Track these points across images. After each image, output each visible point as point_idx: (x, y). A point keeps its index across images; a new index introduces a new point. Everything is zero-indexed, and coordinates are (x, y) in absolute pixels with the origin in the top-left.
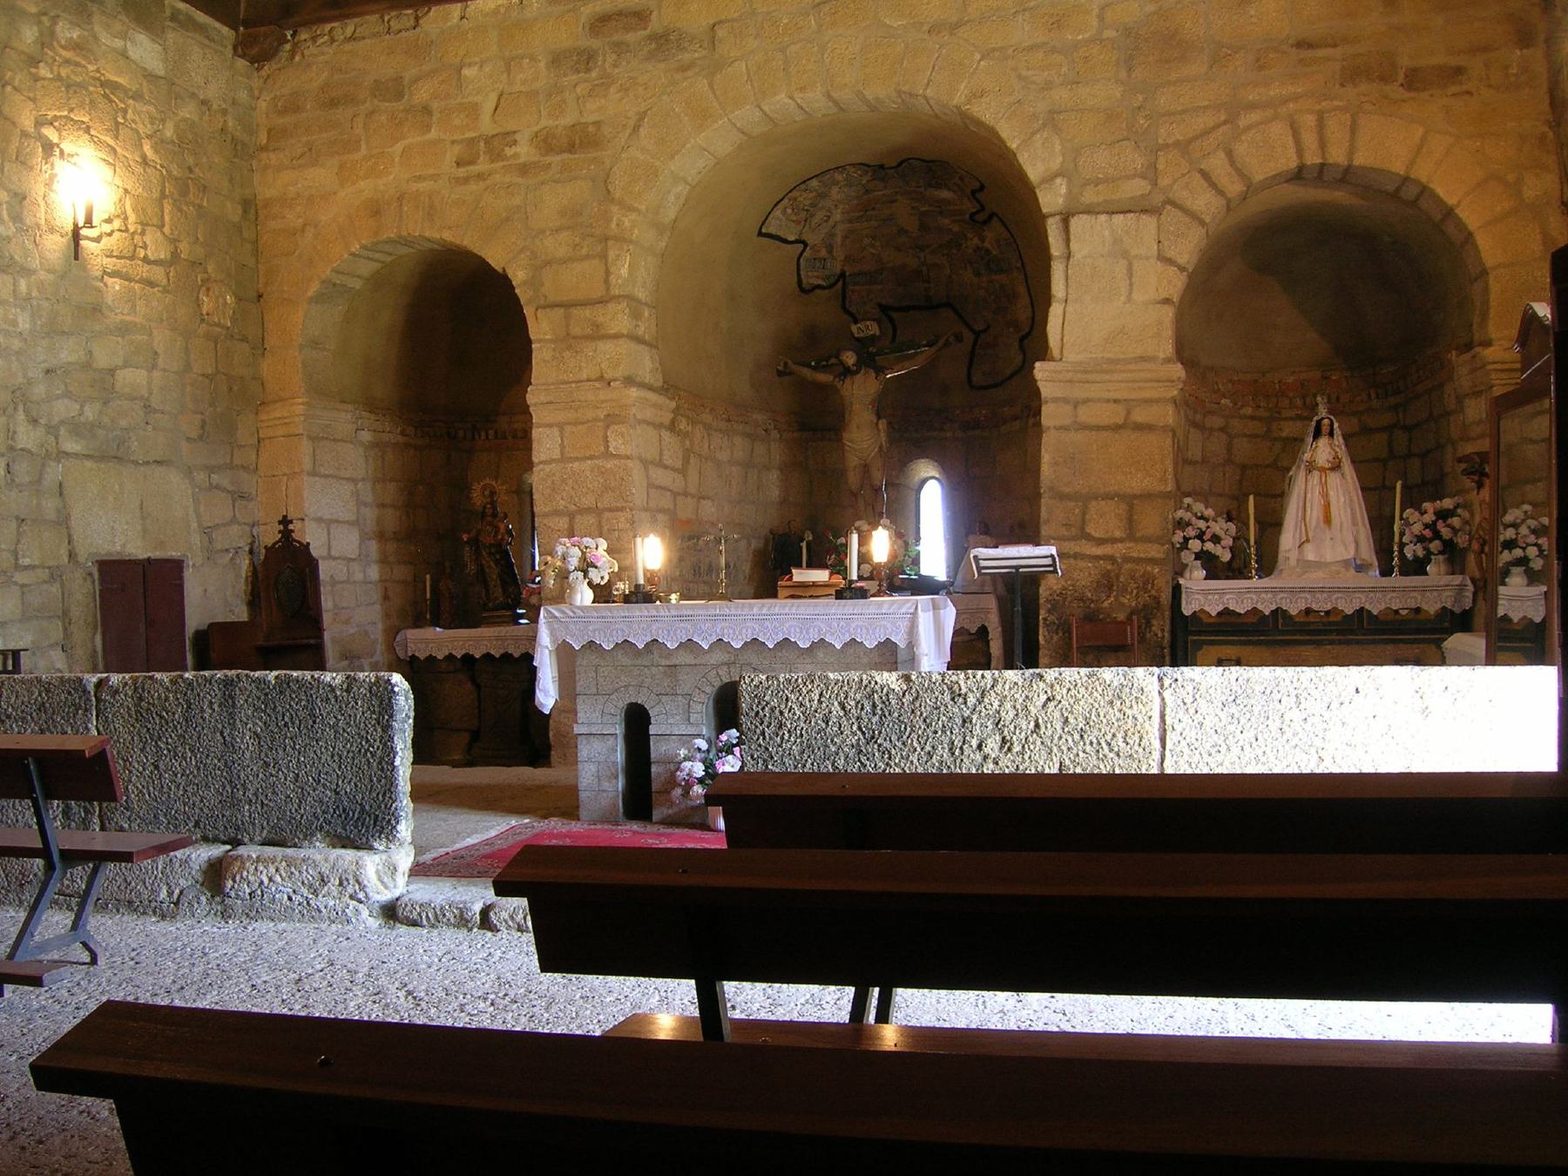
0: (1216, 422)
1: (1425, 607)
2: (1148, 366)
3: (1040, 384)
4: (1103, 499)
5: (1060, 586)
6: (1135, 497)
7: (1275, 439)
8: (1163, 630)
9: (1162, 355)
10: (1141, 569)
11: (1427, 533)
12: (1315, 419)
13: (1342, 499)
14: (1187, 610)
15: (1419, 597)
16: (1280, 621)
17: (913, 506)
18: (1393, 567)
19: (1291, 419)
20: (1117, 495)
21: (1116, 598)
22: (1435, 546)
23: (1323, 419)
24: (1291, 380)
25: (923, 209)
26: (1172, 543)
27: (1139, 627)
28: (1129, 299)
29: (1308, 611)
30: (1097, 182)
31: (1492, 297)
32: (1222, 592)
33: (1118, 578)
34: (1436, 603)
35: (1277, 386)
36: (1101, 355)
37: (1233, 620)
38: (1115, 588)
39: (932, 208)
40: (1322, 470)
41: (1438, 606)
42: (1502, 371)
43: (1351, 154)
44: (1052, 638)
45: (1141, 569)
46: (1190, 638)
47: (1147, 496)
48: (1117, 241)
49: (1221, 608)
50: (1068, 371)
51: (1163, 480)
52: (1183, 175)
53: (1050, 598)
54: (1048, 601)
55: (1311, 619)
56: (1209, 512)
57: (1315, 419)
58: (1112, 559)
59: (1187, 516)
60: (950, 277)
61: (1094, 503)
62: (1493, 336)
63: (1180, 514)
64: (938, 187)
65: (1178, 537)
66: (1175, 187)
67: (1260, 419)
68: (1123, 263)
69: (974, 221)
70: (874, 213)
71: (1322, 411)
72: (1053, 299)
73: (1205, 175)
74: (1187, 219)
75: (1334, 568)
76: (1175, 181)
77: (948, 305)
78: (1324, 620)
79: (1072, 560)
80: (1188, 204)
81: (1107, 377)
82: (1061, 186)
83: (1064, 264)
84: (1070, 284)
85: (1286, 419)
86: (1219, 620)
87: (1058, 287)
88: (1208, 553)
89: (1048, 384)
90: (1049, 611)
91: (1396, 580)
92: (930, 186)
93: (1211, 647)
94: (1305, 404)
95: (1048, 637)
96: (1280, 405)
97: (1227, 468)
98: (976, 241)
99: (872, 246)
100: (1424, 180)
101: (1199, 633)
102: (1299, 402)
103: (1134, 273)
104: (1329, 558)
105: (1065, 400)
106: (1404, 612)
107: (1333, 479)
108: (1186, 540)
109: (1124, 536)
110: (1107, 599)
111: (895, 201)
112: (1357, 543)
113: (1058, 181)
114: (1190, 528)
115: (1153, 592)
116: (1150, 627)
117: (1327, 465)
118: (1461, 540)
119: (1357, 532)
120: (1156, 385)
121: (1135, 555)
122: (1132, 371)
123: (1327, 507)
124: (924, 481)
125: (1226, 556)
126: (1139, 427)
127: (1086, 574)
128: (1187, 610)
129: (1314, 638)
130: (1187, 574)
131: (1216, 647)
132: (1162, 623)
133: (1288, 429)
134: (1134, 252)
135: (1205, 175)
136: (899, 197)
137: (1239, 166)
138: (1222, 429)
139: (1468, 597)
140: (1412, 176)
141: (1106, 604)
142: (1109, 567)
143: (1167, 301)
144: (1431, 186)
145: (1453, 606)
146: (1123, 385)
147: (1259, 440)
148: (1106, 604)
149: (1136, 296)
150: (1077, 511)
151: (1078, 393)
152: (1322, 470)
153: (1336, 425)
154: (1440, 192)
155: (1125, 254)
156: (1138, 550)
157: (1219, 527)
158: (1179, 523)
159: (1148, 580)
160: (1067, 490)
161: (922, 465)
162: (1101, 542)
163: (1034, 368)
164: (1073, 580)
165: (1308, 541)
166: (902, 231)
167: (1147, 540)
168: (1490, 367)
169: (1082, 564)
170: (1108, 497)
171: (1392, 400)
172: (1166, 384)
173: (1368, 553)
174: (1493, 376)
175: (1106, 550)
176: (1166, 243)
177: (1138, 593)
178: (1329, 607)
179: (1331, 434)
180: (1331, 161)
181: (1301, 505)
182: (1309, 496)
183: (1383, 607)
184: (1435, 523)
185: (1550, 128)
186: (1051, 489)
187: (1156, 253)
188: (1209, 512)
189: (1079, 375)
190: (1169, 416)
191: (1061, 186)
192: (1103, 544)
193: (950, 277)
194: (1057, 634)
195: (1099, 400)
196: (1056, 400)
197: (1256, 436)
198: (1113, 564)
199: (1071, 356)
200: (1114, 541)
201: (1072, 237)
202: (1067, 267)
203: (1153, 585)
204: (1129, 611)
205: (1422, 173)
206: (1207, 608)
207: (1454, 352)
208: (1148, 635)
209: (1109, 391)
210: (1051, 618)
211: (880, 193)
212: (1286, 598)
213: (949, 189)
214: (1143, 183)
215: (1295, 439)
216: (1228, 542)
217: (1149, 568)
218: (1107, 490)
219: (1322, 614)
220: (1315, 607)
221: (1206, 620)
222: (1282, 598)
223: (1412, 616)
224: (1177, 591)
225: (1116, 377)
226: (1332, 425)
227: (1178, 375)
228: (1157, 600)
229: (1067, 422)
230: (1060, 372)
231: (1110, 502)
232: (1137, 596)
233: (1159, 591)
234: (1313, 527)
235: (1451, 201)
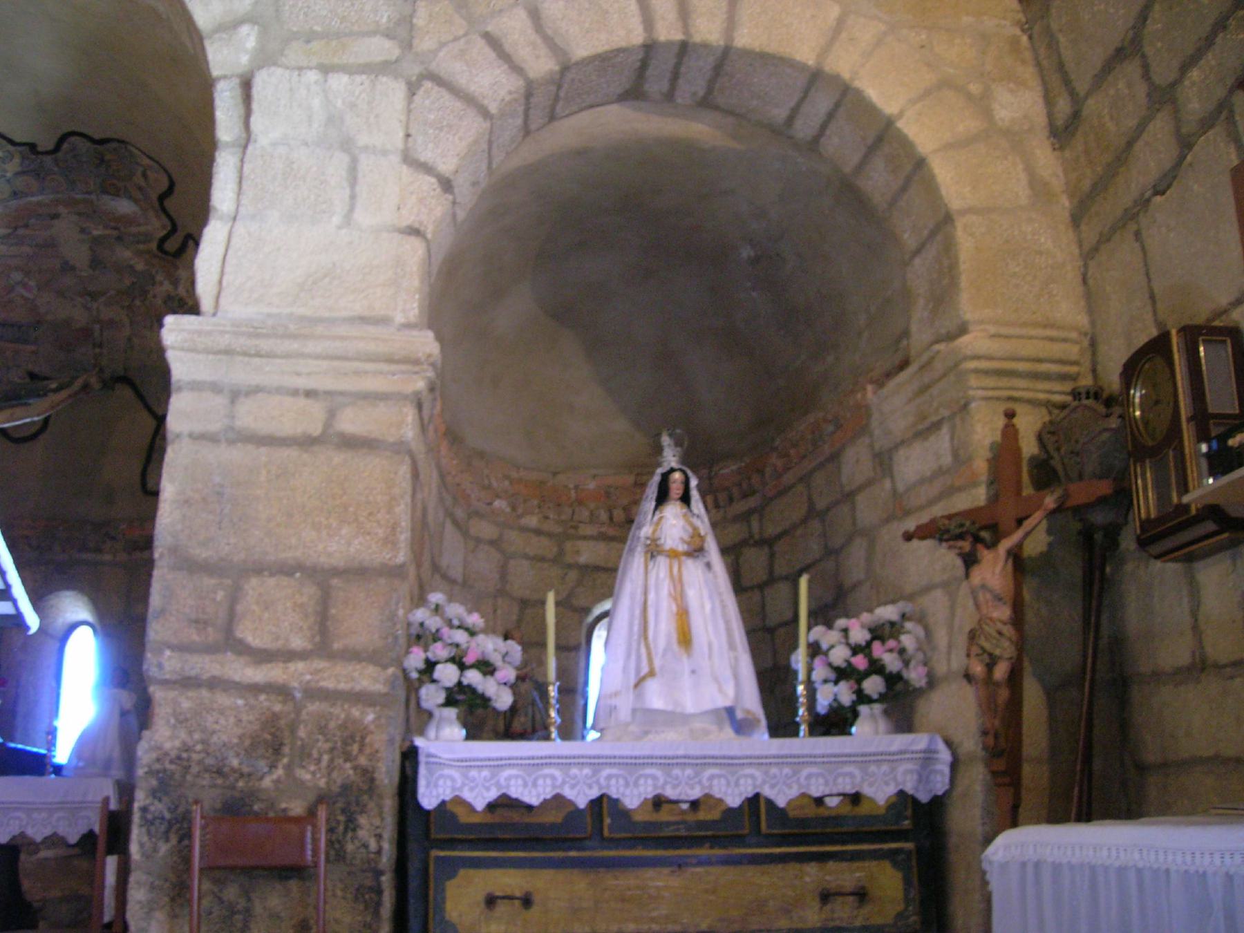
0: (486, 530)
1: (867, 791)
2: (372, 330)
3: (171, 356)
4: (272, 575)
5: (177, 743)
6: (336, 572)
7: (570, 566)
8: (379, 837)
9: (399, 318)
10: (339, 712)
11: (860, 662)
12: (659, 471)
13: (708, 607)
14: (428, 798)
15: (857, 772)
16: (607, 821)
17: (52, 660)
18: (798, 725)
19: (592, 538)
20: (300, 567)
21: (289, 768)
22: (873, 685)
23: (672, 470)
24: (592, 485)
25: (96, 233)
26: (404, 670)
27: (331, 830)
28: (348, 220)
29: (658, 802)
30: (310, 37)
31: (963, 256)
32: (497, 765)
33: (293, 729)
34: (887, 784)
35: (573, 492)
36: (288, 310)
37: (515, 817)
38: (286, 750)
39: (108, 232)
40: (673, 555)
41: (891, 790)
42: (986, 373)
43: (731, 24)
44: (155, 850)
45: (339, 712)
46: (435, 853)
47: (359, 573)
48: (333, 120)
49: (492, 795)
50: (223, 333)
51: (390, 541)
52: (456, 39)
53: (157, 766)
54: (151, 773)
55: (664, 816)
56: (475, 619)
57: (659, 471)
58: (282, 691)
59: (433, 623)
60: (129, 339)
61: (254, 581)
62: (968, 316)
63: (420, 614)
64: (117, 193)
65: (415, 660)
66: (441, 54)
67: (550, 535)
68: (341, 160)
69: (166, 253)
70: (27, 232)
71: (671, 458)
72: (212, 215)
73: (493, 42)
74: (459, 105)
75: (697, 725)
76: (442, 45)
77: (125, 380)
78: (691, 818)
79: (205, 693)
80: (462, 80)
81: (295, 346)
82: (249, 37)
83: (239, 155)
84: (245, 186)
85: (585, 538)
86: (489, 819)
87: (223, 194)
88: (470, 690)
89: (179, 353)
90: (154, 793)
91: (804, 744)
92: (105, 191)
93: (471, 872)
94: (611, 519)
95: (148, 845)
96: (576, 517)
97: (500, 601)
98: (167, 287)
99: (25, 286)
100: (846, 75)
101: (451, 843)
102: (604, 516)
103: (360, 175)
104: (690, 705)
105: (216, 388)
106: (832, 802)
107: (693, 571)
108: (430, 665)
109: (310, 647)
110: (270, 772)
111: (55, 216)
112: (736, 676)
113: (245, 29)
114: (439, 644)
115: (363, 761)
116: (354, 830)
117: (682, 548)
118: (916, 676)
119: (736, 659)
120: (385, 367)
121: (329, 684)
122: (342, 338)
123: (683, 615)
124: (73, 627)
125: (503, 700)
126: (350, 443)
127: (232, 720)
128: (428, 798)
129: (886, 846)
130: (431, 732)
131: (482, 873)
132: (377, 822)
133: (588, 553)
134: (363, 140)
135: (493, 42)
136: (62, 209)
137: (549, 32)
138: (492, 543)
139: (941, 772)
140: (827, 69)
141: (267, 782)
142: (278, 708)
143: (414, 231)
144: (857, 84)
145: (916, 789)
146: (325, 364)
147: (546, 565)
148: (267, 782)
149: (360, 216)
150: (220, 595)
151: (241, 374)
152: (673, 555)
153: (694, 482)
154: (873, 94)
155: (347, 145)
156: (338, 676)
157: (490, 646)
158: (419, 637)
159: (353, 736)
160: (202, 554)
161: (67, 601)
162: (263, 656)
163: (161, 325)
164: (204, 730)
165: (652, 673)
166: (67, 268)
167: (353, 656)
168: (972, 365)
169: (223, 700)
170: (285, 570)
171: (740, 507)
172: (403, 367)
173: (751, 701)
174: (973, 381)
175: (273, 673)
176: (420, 139)
177: (332, 760)
178: (696, 793)
179: (685, 499)
180: (697, 39)
181: (638, 612)
182: (652, 597)
183: (794, 792)
184: (869, 644)
185: (1023, 30)
186: (174, 550)
187: (400, 144)
188: (475, 619)
189: (242, 340)
190: (406, 426)
191: (249, 37)
192: (270, 661)
193: (129, 339)
194: (167, 840)
195: (280, 390)
196: (196, 386)
197: (542, 559)
198: (284, 702)
199: (236, 309)
200: (289, 656)
201: (255, 106)
202: (242, 161)
203: (362, 746)
204: (311, 797)
205: (842, 64)
206: (467, 795)
207: (870, 388)
208: (350, 847)
209: (298, 374)
210: (158, 807)
211: (34, 199)
212: (617, 776)
213: (130, 198)
214: (387, 44)
215: (597, 568)
216: (509, 674)
217: (356, 712)
218: (283, 556)
219: (685, 806)
220: (670, 793)
221: (464, 818)
222: (609, 777)
223: (847, 809)
224: (410, 756)
225: (311, 347)
226: (687, 483)
227: (428, 351)
228: (368, 775)
229: (215, 426)
230: (209, 333)
231: (285, 581)
232: (331, 768)
233: (373, 756)
234: (660, 651)
235: (889, 108)
